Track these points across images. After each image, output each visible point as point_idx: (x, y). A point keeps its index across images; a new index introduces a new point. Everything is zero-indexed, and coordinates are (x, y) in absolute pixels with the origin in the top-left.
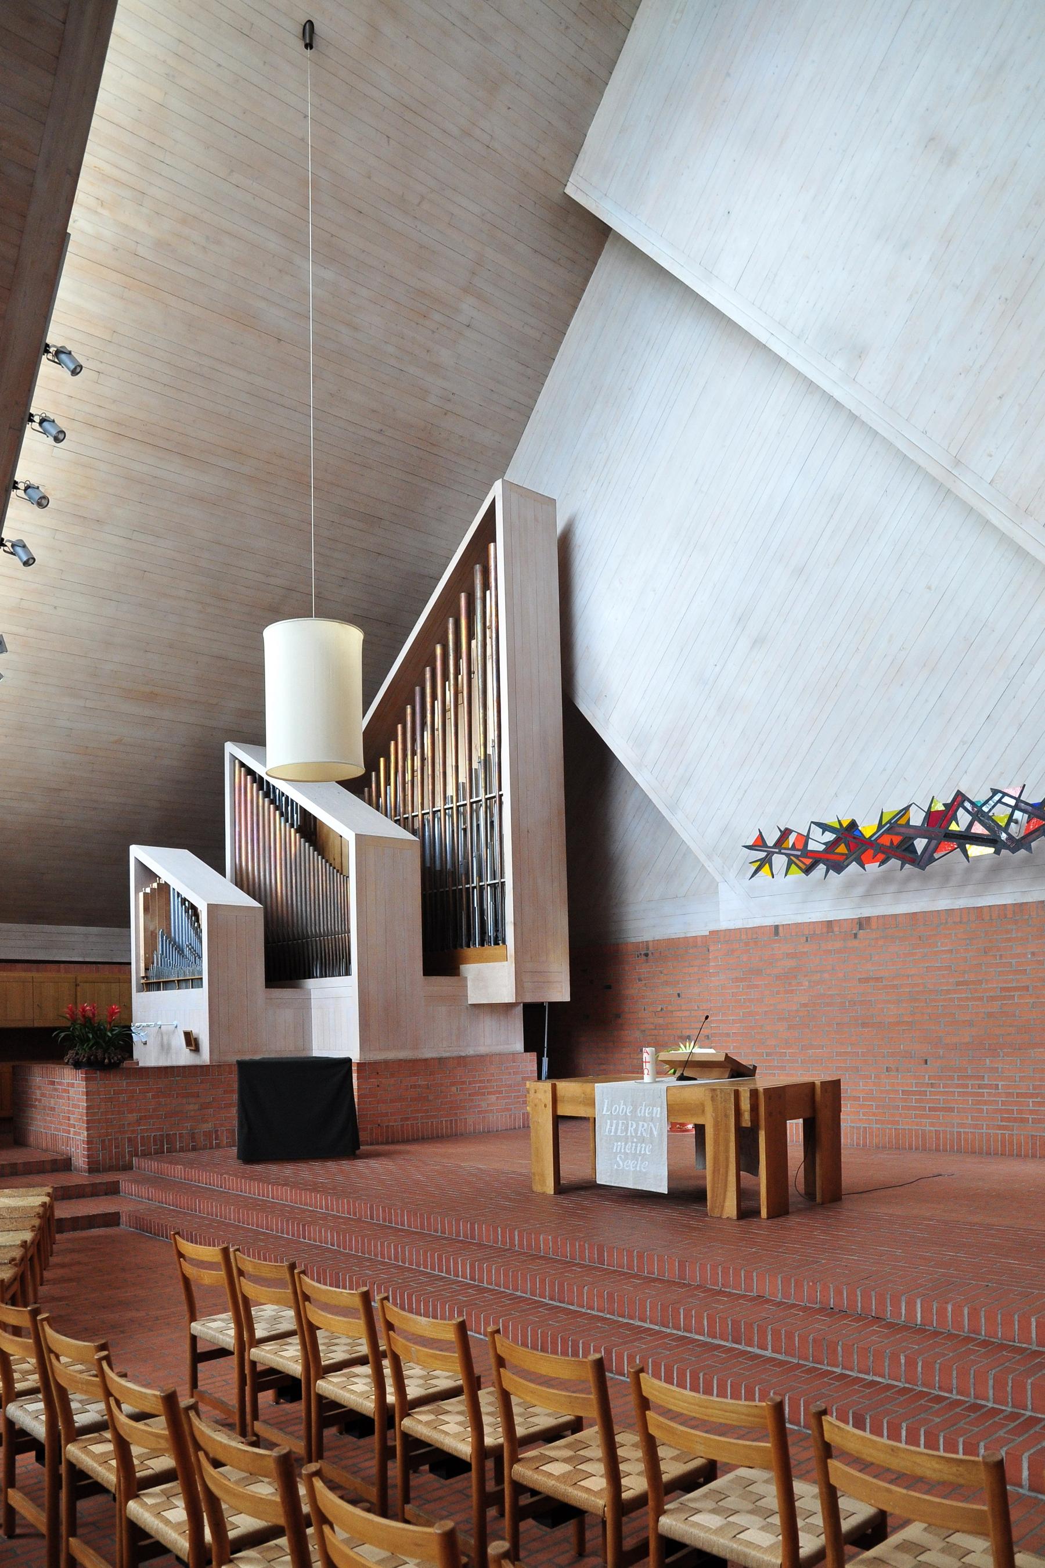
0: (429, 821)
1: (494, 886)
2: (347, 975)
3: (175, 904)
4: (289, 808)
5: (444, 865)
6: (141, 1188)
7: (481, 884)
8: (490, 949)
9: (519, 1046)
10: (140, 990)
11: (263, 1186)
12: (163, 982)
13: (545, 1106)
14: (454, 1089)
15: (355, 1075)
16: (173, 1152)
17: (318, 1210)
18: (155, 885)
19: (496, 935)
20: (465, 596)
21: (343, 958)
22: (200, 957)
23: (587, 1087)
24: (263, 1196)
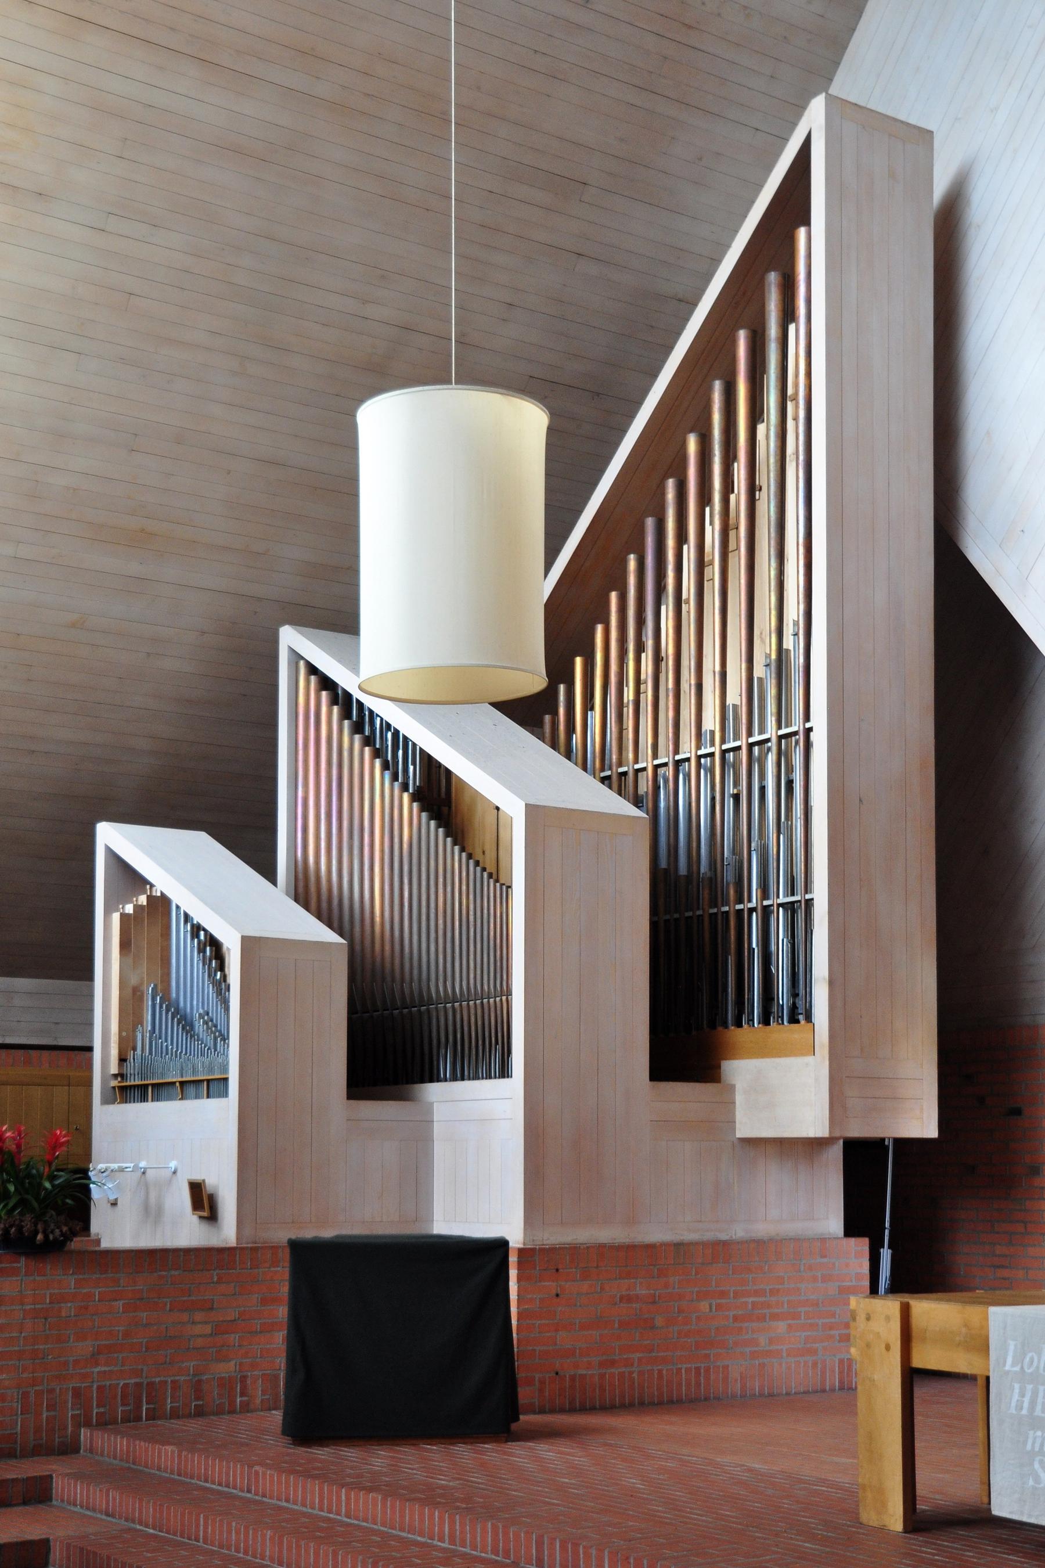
0: (666, 781)
1: (791, 908)
2: (503, 1077)
3: (179, 936)
4: (400, 753)
5: (695, 868)
6: (95, 1493)
7: (766, 903)
8: (781, 1032)
9: (834, 1223)
10: (107, 1101)
11: (330, 1492)
12: (153, 1085)
13: (888, 1348)
14: (704, 1306)
15: (513, 1273)
16: (159, 1418)
17: (435, 1542)
18: (143, 900)
19: (794, 1004)
20: (747, 337)
21: (497, 1043)
22: (225, 1038)
23: (973, 1312)
24: (330, 1511)
